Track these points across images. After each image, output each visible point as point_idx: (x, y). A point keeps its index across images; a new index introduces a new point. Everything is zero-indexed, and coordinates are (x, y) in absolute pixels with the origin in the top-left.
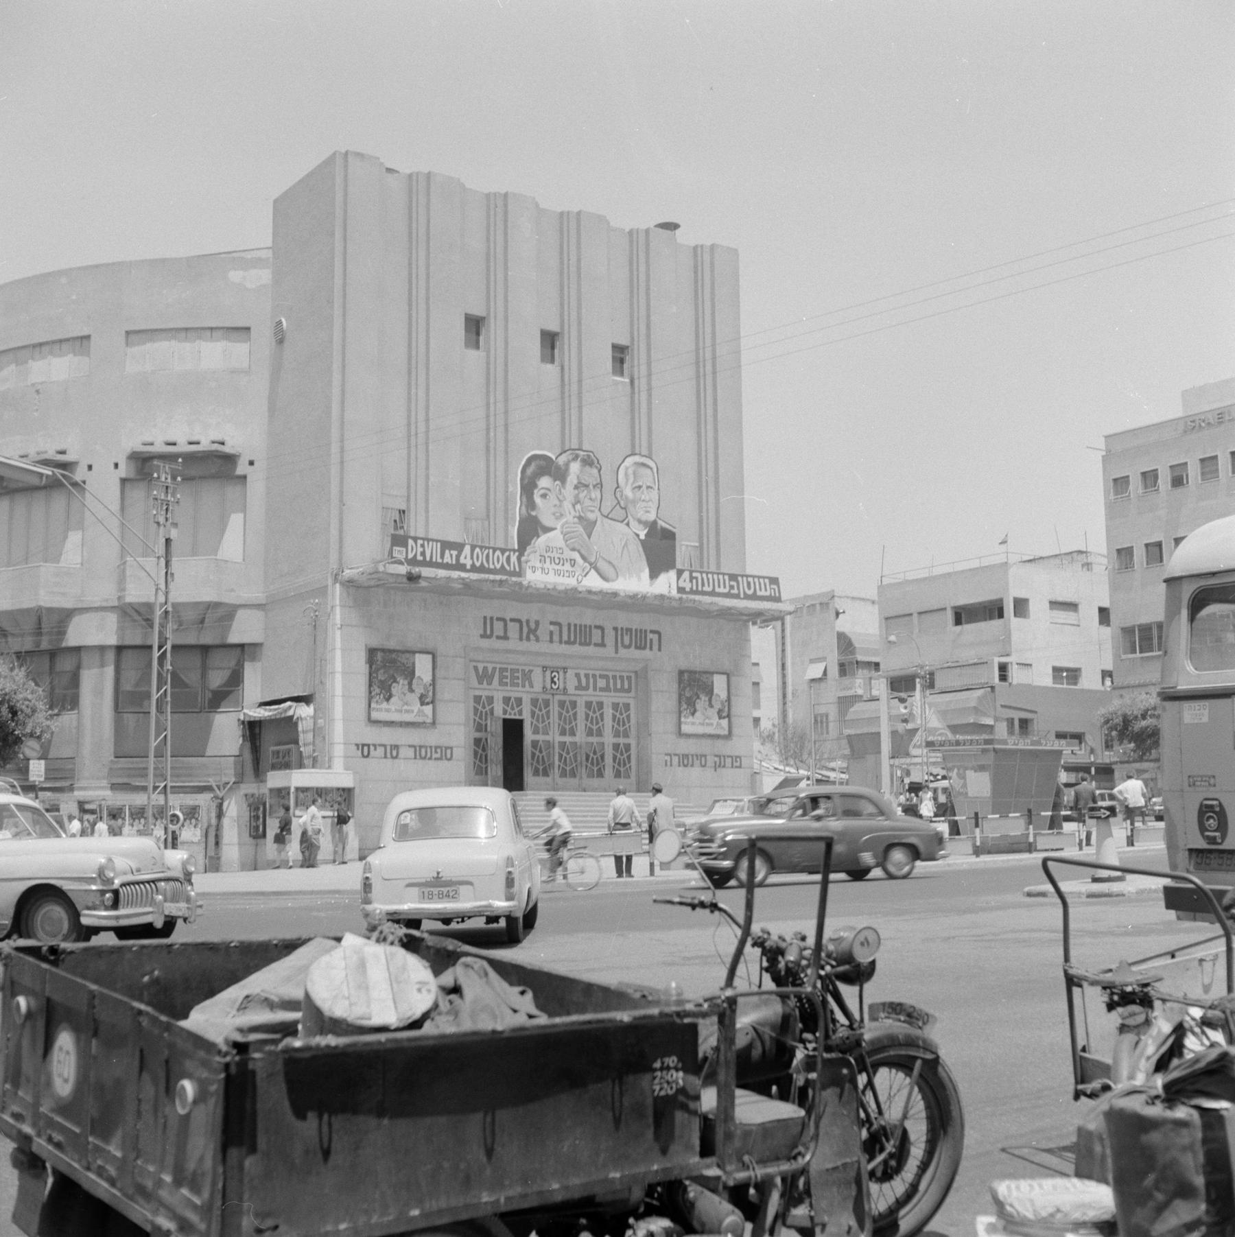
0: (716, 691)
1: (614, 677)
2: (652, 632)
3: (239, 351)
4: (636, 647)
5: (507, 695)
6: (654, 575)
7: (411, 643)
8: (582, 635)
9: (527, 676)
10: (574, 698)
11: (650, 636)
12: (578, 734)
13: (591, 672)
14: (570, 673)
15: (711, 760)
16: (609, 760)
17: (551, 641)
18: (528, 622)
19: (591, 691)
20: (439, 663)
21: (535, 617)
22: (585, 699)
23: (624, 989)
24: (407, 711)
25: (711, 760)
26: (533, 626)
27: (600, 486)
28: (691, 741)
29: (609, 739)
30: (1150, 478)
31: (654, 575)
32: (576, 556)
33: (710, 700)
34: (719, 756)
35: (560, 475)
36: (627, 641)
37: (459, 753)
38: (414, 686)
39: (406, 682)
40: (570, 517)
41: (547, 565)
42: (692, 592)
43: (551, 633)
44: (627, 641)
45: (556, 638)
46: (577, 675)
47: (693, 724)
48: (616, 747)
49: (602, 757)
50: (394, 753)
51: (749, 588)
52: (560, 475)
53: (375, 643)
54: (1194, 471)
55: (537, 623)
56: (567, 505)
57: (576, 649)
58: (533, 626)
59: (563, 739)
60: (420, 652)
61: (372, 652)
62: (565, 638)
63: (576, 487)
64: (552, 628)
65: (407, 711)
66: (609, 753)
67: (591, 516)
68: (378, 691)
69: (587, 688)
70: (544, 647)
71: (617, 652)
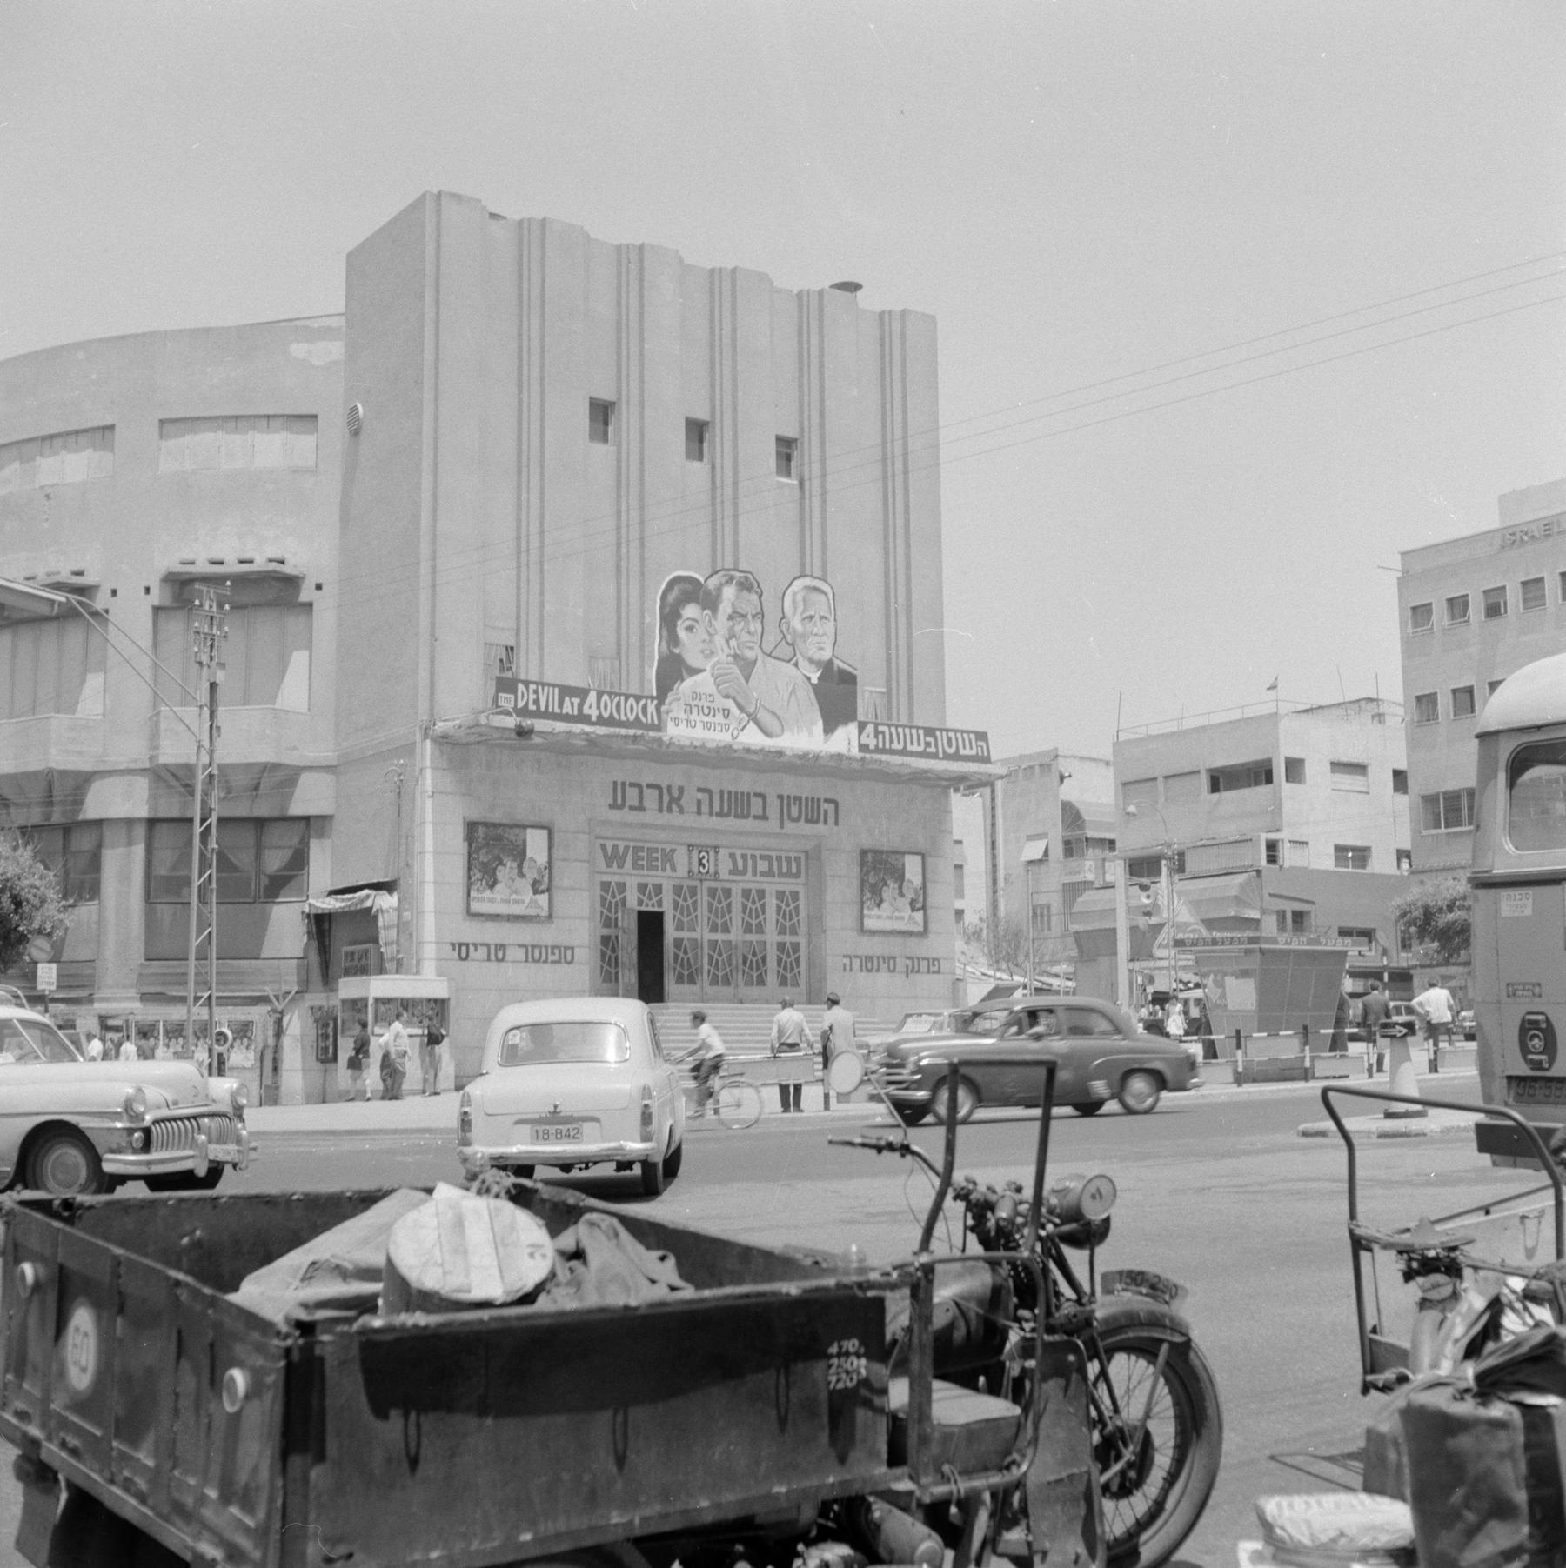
0: (907, 876)
1: (779, 858)
2: (826, 801)
3: (303, 444)
4: (807, 821)
5: (643, 880)
6: (829, 729)
7: (521, 815)
8: (737, 805)
9: (668, 857)
10: (728, 885)
11: (824, 806)
12: (733, 930)
13: (749, 852)
14: (723, 853)
15: (901, 964)
16: (772, 963)
17: (699, 812)
18: (669, 788)
19: (749, 876)
20: (556, 840)
21: (678, 782)
22: (742, 885)
24: (516, 902)
25: (901, 964)
26: (675, 793)
27: (760, 615)
28: (876, 939)
29: (772, 937)
30: (1458, 606)
31: (829, 729)
32: (730, 704)
33: (900, 887)
34: (912, 959)
35: (710, 602)
36: (795, 813)
37: (582, 954)
38: (525, 870)
39: (515, 865)
40: (723, 656)
41: (694, 716)
42: (877, 750)
43: (699, 802)
44: (795, 813)
45: (705, 808)
46: (732, 856)
47: (879, 917)
48: (781, 947)
49: (764, 959)
50: (500, 955)
51: (950, 745)
52: (710, 602)
53: (475, 816)
54: (1513, 597)
55: (681, 790)
56: (719, 640)
57: (731, 823)
58: (675, 793)
59: (714, 936)
60: (532, 827)
61: (471, 827)
62: (717, 808)
63: (731, 618)
64: (700, 796)
65: (516, 902)
66: (772, 955)
67: (750, 654)
68: (479, 875)
69: (744, 872)
70: (689, 820)
71: (782, 826)
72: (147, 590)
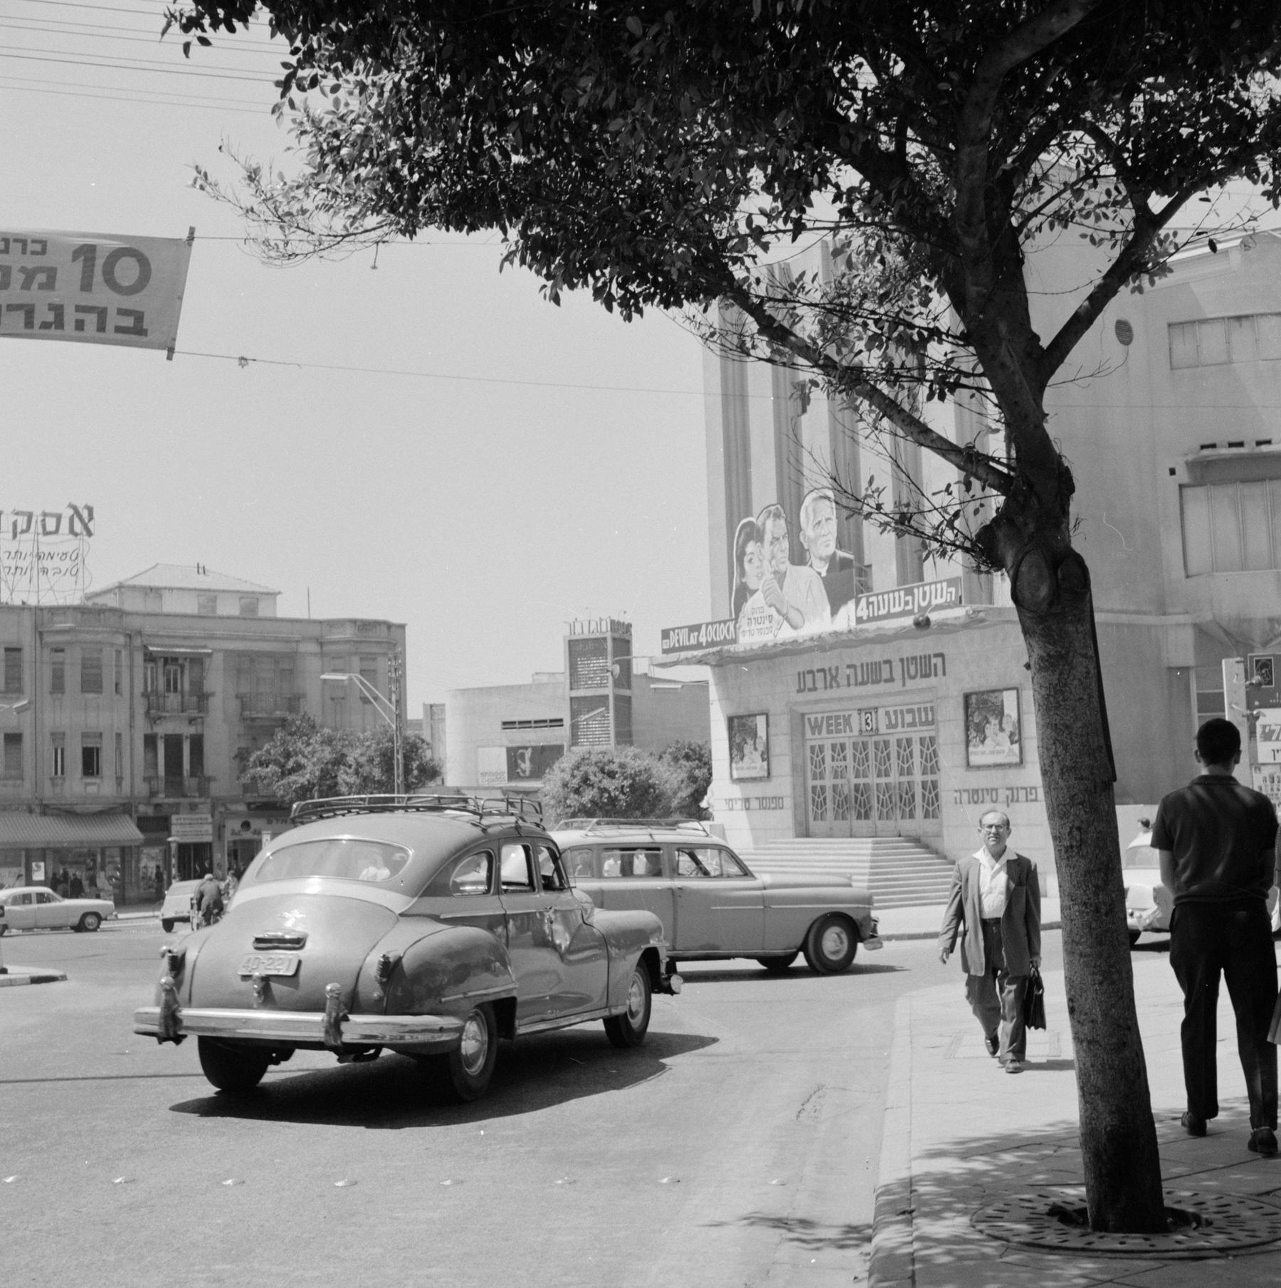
0: (1006, 712)
1: (919, 709)
4: (922, 676)
5: (834, 741)
7: (993, 683)
8: (873, 673)
9: (847, 720)
10: (886, 738)
11: (934, 661)
13: (898, 708)
14: (881, 712)
15: (1003, 794)
16: (918, 799)
19: (900, 729)
20: (771, 722)
21: (835, 663)
22: (897, 736)
23: (427, 963)
24: (998, 752)
25: (1003, 794)
26: (834, 672)
28: (981, 773)
29: (918, 777)
31: (834, 612)
32: (773, 611)
33: (1000, 723)
34: (1012, 789)
36: (913, 672)
37: (788, 802)
38: (1004, 726)
39: (997, 722)
41: (753, 627)
42: (870, 619)
43: (848, 677)
44: (913, 672)
45: (852, 681)
46: (887, 713)
47: (983, 753)
48: (924, 784)
49: (913, 796)
51: (924, 599)
53: (732, 712)
55: (837, 668)
56: (766, 563)
58: (834, 672)
62: (860, 679)
63: (772, 543)
64: (848, 671)
65: (998, 752)
66: (918, 791)
67: (782, 568)
68: (974, 734)
69: (895, 726)
70: (843, 692)
71: (904, 685)
72: (1172, 472)
